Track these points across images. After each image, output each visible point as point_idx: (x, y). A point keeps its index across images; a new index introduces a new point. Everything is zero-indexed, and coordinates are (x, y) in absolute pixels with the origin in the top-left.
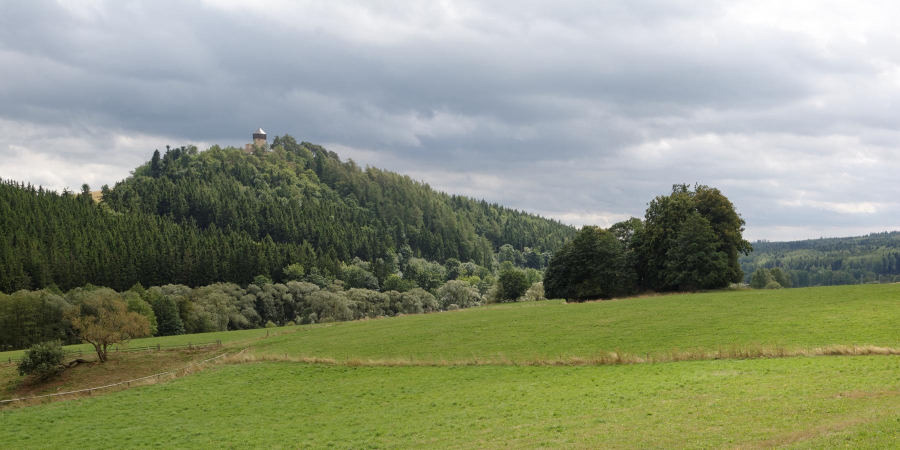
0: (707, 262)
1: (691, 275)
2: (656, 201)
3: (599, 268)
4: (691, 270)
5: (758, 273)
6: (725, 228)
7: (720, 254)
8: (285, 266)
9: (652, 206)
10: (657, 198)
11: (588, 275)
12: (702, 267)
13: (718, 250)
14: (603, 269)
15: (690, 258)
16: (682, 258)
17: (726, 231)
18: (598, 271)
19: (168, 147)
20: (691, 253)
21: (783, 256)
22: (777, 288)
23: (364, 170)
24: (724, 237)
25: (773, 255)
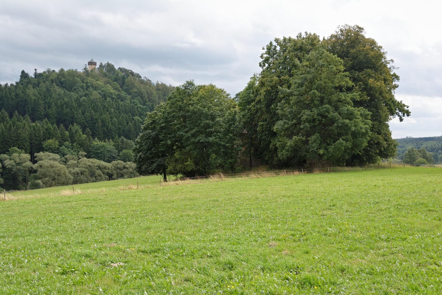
0: (333, 121)
1: (307, 142)
2: (274, 43)
3: (189, 134)
4: (308, 135)
5: (409, 152)
6: (370, 76)
7: (358, 111)
8: (44, 140)
9: (268, 52)
10: (277, 40)
11: (180, 143)
12: (325, 128)
13: (357, 104)
14: (193, 135)
15: (306, 114)
16: (295, 115)
17: (371, 81)
18: (188, 139)
19: (36, 70)
20: (308, 107)
21: (421, 145)
22: (424, 163)
23: (155, 84)
24: (367, 89)
25: (415, 144)
